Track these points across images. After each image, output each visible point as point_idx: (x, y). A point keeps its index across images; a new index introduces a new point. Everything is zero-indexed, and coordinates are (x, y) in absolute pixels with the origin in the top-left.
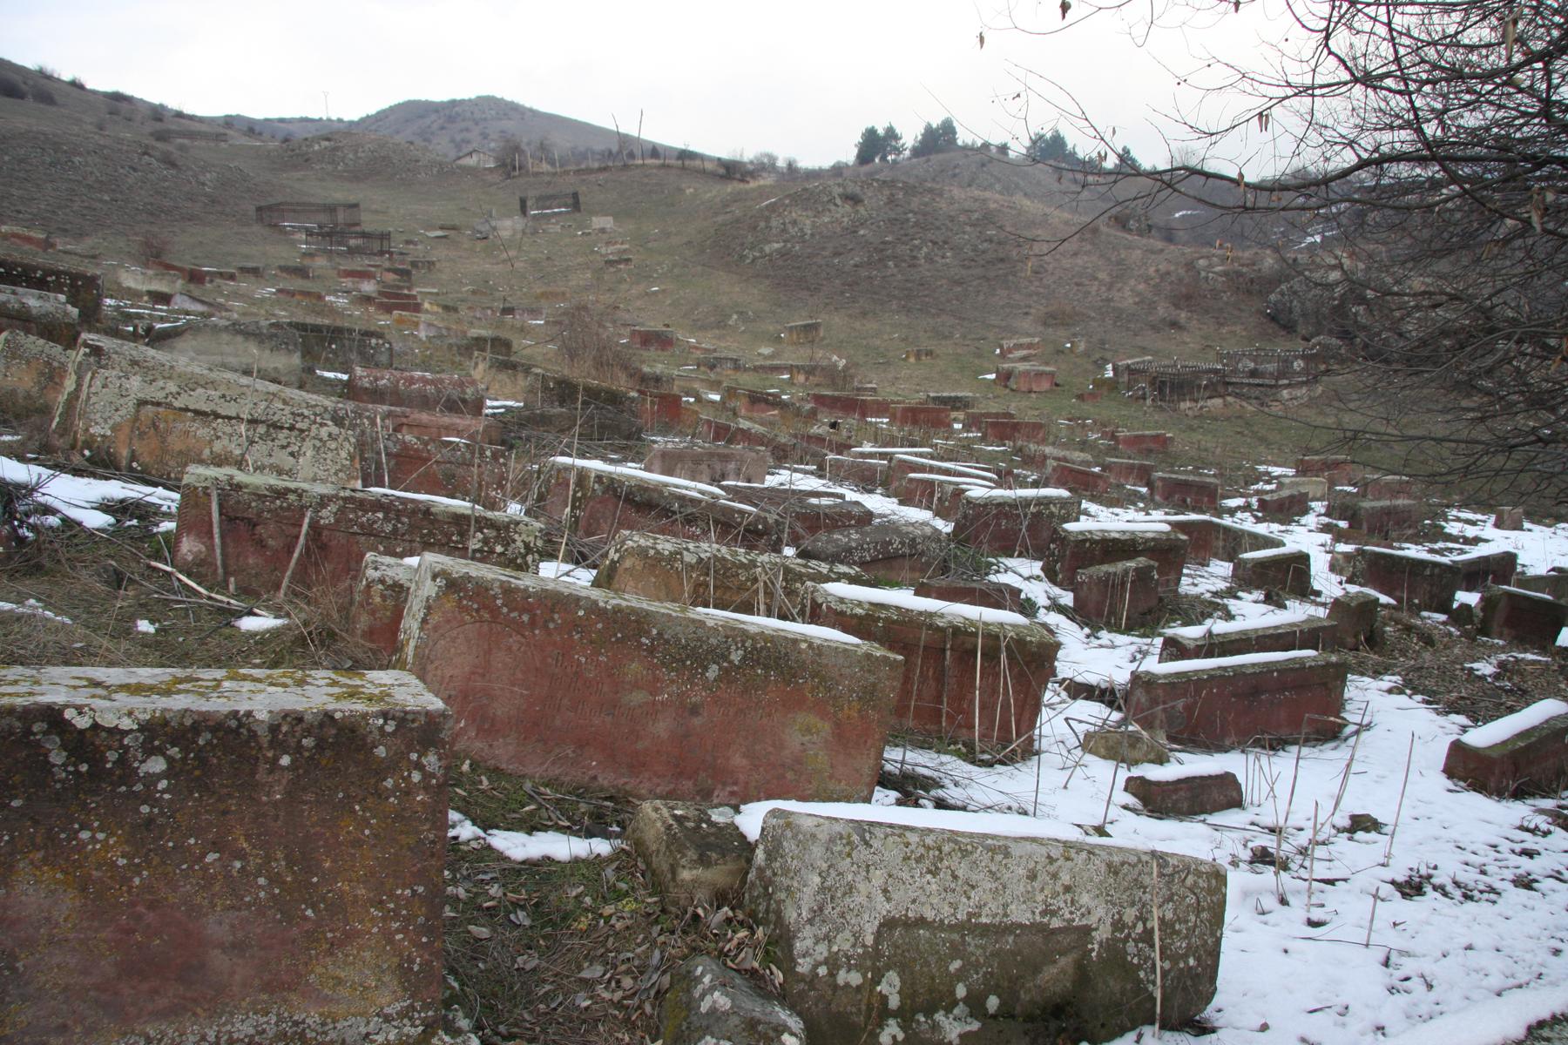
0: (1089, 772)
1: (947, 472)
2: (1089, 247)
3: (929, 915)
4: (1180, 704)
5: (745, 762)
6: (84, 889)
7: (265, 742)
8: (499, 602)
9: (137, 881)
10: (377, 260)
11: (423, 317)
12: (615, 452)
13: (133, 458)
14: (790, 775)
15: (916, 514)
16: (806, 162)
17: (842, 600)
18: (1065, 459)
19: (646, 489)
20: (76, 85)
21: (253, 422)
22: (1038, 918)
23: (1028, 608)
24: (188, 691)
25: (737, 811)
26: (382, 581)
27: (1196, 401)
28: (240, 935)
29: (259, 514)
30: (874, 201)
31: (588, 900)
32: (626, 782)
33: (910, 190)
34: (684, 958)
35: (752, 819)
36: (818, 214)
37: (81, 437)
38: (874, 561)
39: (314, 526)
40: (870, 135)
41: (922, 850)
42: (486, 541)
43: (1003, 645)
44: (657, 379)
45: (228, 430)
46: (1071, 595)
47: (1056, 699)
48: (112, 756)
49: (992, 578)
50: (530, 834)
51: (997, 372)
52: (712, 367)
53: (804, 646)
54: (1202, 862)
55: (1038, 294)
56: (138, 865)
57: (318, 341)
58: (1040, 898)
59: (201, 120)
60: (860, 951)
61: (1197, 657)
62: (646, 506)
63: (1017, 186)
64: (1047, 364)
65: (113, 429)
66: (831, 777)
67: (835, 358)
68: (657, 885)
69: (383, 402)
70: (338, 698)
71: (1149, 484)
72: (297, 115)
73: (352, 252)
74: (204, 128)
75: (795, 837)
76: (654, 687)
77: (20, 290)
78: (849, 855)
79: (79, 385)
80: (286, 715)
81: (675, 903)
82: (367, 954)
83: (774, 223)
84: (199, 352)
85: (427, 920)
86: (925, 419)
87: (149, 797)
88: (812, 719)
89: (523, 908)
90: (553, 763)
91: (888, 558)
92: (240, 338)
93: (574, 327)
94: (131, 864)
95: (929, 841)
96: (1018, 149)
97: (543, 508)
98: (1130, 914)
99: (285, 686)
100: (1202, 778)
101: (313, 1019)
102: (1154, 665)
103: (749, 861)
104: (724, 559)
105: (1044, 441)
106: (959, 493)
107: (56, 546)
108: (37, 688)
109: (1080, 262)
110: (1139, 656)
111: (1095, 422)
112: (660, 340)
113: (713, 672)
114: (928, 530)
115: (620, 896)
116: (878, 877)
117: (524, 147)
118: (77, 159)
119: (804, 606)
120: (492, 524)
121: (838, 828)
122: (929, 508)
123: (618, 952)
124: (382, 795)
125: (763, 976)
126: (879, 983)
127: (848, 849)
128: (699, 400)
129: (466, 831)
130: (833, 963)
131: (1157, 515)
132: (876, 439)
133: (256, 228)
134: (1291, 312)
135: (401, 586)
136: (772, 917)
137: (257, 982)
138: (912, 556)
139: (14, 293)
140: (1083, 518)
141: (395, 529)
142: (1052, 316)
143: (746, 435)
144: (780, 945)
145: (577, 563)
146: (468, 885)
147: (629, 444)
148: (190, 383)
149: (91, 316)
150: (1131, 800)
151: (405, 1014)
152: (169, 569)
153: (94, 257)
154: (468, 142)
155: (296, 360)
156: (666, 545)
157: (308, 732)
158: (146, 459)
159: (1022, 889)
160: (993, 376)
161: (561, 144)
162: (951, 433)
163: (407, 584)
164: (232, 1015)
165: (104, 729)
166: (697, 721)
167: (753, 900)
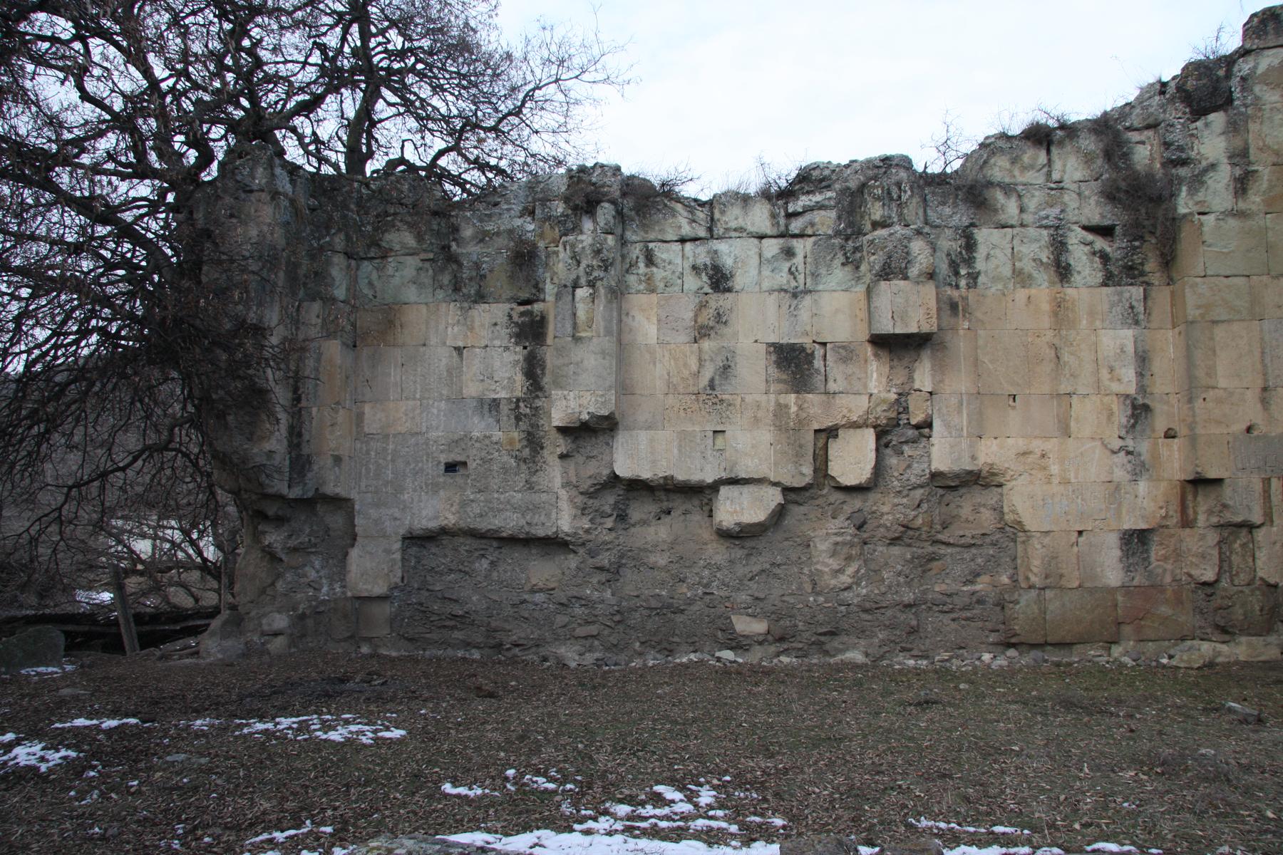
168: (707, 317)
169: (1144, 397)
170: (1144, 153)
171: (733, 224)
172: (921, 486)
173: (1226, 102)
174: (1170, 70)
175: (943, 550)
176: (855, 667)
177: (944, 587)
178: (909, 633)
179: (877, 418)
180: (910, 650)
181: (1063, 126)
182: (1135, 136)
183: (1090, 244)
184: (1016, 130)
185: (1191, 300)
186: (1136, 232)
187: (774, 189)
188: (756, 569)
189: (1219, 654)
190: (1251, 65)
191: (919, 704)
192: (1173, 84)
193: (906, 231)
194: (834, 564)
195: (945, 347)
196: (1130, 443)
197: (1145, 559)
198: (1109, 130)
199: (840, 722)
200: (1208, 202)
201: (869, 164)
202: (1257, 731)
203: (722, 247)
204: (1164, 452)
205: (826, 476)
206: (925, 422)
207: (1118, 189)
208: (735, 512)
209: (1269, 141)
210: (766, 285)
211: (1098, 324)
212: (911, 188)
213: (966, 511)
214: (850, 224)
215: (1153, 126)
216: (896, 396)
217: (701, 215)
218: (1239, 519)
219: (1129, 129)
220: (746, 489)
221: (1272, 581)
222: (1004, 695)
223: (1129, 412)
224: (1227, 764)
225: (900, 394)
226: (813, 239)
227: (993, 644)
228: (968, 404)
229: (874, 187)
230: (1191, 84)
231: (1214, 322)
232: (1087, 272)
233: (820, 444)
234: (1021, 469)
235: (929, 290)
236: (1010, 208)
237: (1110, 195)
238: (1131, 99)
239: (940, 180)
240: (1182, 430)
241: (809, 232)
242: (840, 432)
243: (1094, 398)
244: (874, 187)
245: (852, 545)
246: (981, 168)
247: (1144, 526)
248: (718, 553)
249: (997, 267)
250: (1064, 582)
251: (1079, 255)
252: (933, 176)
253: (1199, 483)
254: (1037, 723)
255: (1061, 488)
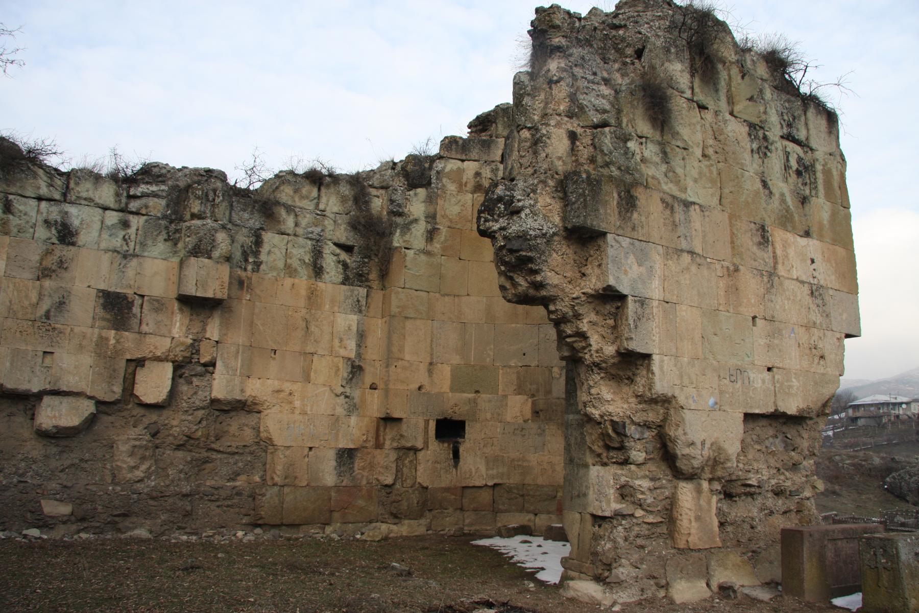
134: (901, 488)
168: (50, 262)
169: (359, 361)
170: (378, 204)
171: (84, 195)
172: (203, 408)
173: (427, 184)
174: (400, 156)
175: (215, 455)
176: (141, 541)
177: (213, 482)
178: (185, 516)
179: (176, 356)
180: (184, 528)
181: (331, 175)
182: (374, 192)
183: (337, 255)
184: (300, 171)
185: (394, 302)
186: (367, 253)
187: (121, 175)
188: (67, 463)
189: (392, 531)
190: (443, 165)
191: (186, 569)
192: (400, 165)
193: (215, 225)
194: (132, 462)
195: (231, 311)
196: (348, 390)
197: (351, 468)
198: (359, 184)
199: (122, 584)
200: (410, 241)
201: (196, 172)
202: (405, 581)
203: (73, 210)
204: (369, 398)
205: (132, 395)
206: (211, 362)
207: (359, 223)
208: (55, 417)
209: (448, 212)
210: (103, 245)
211: (336, 309)
212: (223, 195)
213: (234, 428)
214: (175, 212)
215: (385, 188)
216: (191, 341)
217: (59, 182)
218: (409, 445)
219: (371, 186)
220: (66, 400)
221: (425, 485)
222: (249, 561)
223: (349, 370)
224: (386, 602)
225: (194, 340)
226: (145, 218)
227: (245, 524)
228: (243, 352)
229: (197, 189)
230: (410, 167)
231: (406, 318)
232: (333, 273)
233: (130, 370)
234: (275, 401)
235: (225, 269)
236: (290, 222)
237: (354, 226)
238: (375, 168)
239: (243, 194)
240: (381, 385)
241: (144, 211)
242: (147, 363)
243: (328, 358)
244: (197, 189)
245: (146, 448)
246: (274, 191)
247: (352, 446)
248: (35, 449)
249: (275, 260)
250: (297, 482)
251: (329, 262)
252: (240, 189)
253: (389, 420)
254: (269, 581)
255: (301, 417)
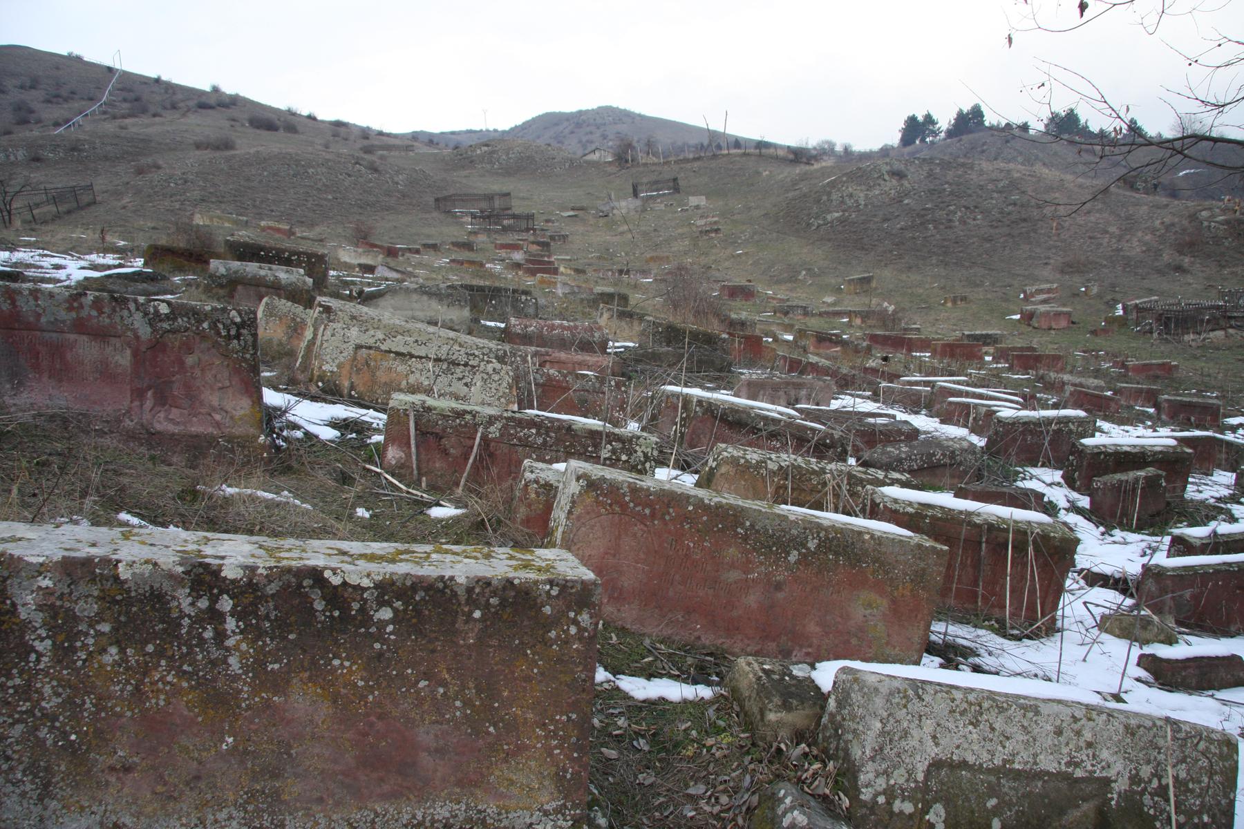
0: (1105, 648)
1: (981, 396)
2: (1100, 206)
3: (971, 759)
4: (1187, 594)
5: (818, 629)
6: (335, 702)
7: (463, 599)
8: (627, 499)
9: (371, 698)
10: (524, 236)
11: (560, 278)
12: (711, 382)
13: (352, 387)
14: (854, 641)
15: (954, 431)
16: (859, 146)
17: (896, 501)
18: (1081, 385)
19: (737, 411)
20: (311, 118)
21: (438, 360)
22: (1063, 768)
23: (1050, 509)
24: (407, 561)
25: (814, 668)
26: (536, 482)
27: (1199, 334)
28: (442, 742)
29: (444, 430)
30: (916, 175)
31: (694, 732)
32: (723, 642)
33: (946, 165)
34: (770, 782)
35: (825, 675)
36: (870, 188)
37: (316, 373)
38: (921, 469)
39: (484, 438)
40: (912, 121)
41: (965, 705)
42: (614, 451)
43: (1030, 539)
44: (743, 324)
45: (420, 366)
46: (1087, 499)
47: (1075, 586)
48: (356, 606)
49: (1019, 484)
50: (648, 679)
51: (1021, 313)
52: (786, 314)
53: (867, 537)
54: (1213, 731)
55: (1056, 247)
56: (372, 687)
57: (482, 298)
58: (1065, 750)
59: (396, 136)
60: (913, 785)
61: (1203, 553)
62: (737, 425)
63: (1037, 158)
64: (1064, 305)
65: (339, 366)
66: (887, 643)
67: (886, 304)
68: (749, 724)
69: (531, 344)
70: (516, 569)
71: (1156, 405)
72: (464, 129)
73: (505, 229)
74: (397, 142)
75: (861, 689)
76: (746, 568)
77: (274, 267)
78: (905, 706)
79: (315, 335)
80: (479, 581)
81: (763, 739)
82: (533, 763)
83: (834, 197)
84: (396, 309)
85: (578, 740)
86: (961, 353)
87: (380, 637)
88: (873, 596)
89: (643, 737)
90: (667, 625)
91: (932, 467)
92: (425, 298)
93: (679, 285)
94: (367, 686)
95: (971, 698)
96: (1037, 127)
97: (656, 426)
98: (1146, 771)
99: (476, 558)
100: (1209, 658)
101: (492, 810)
102: (1161, 559)
103: (823, 708)
104: (800, 467)
105: (1062, 370)
106: (991, 413)
107: (302, 452)
108: (304, 555)
109: (1092, 219)
110: (1148, 552)
111: (1107, 354)
112: (745, 293)
113: (794, 556)
114: (965, 444)
115: (719, 731)
116: (929, 725)
117: (635, 144)
118: (310, 171)
119: (865, 505)
120: (619, 438)
121: (896, 684)
122: (965, 426)
123: (717, 775)
124: (547, 643)
125: (833, 801)
126: (927, 813)
127: (904, 701)
128: (776, 340)
129: (601, 675)
130: (890, 793)
131: (1164, 431)
132: (922, 368)
133: (435, 214)
135: (551, 485)
136: (841, 754)
137: (453, 778)
138: (951, 465)
139: (270, 269)
140: (1097, 434)
141: (545, 442)
142: (1069, 265)
143: (814, 368)
144: (847, 777)
145: (683, 469)
146: (602, 717)
147: (721, 375)
148: (393, 332)
149: (321, 284)
150: (1143, 673)
151: (559, 811)
152: (378, 470)
153: (321, 240)
154: (592, 142)
155: (466, 313)
156: (753, 455)
157: (494, 593)
158: (361, 388)
159: (1050, 742)
160: (1018, 317)
161: (664, 141)
162: (982, 365)
163: (556, 484)
164: (434, 801)
165: (350, 585)
166: (780, 595)
167: (825, 739)
